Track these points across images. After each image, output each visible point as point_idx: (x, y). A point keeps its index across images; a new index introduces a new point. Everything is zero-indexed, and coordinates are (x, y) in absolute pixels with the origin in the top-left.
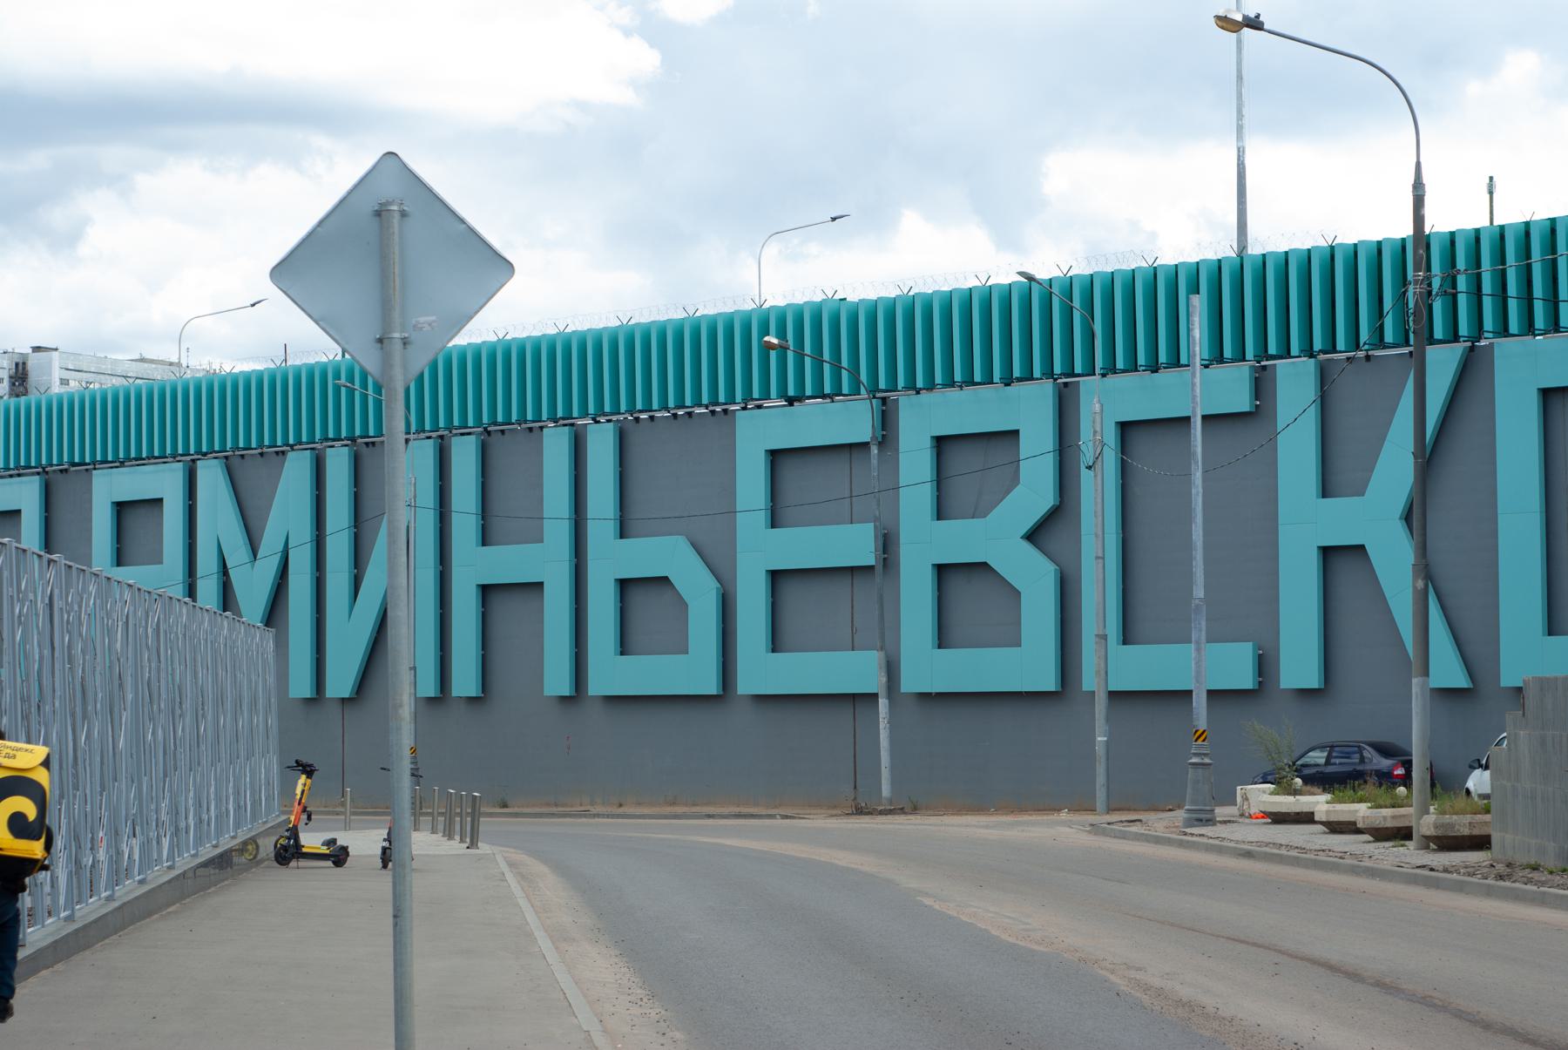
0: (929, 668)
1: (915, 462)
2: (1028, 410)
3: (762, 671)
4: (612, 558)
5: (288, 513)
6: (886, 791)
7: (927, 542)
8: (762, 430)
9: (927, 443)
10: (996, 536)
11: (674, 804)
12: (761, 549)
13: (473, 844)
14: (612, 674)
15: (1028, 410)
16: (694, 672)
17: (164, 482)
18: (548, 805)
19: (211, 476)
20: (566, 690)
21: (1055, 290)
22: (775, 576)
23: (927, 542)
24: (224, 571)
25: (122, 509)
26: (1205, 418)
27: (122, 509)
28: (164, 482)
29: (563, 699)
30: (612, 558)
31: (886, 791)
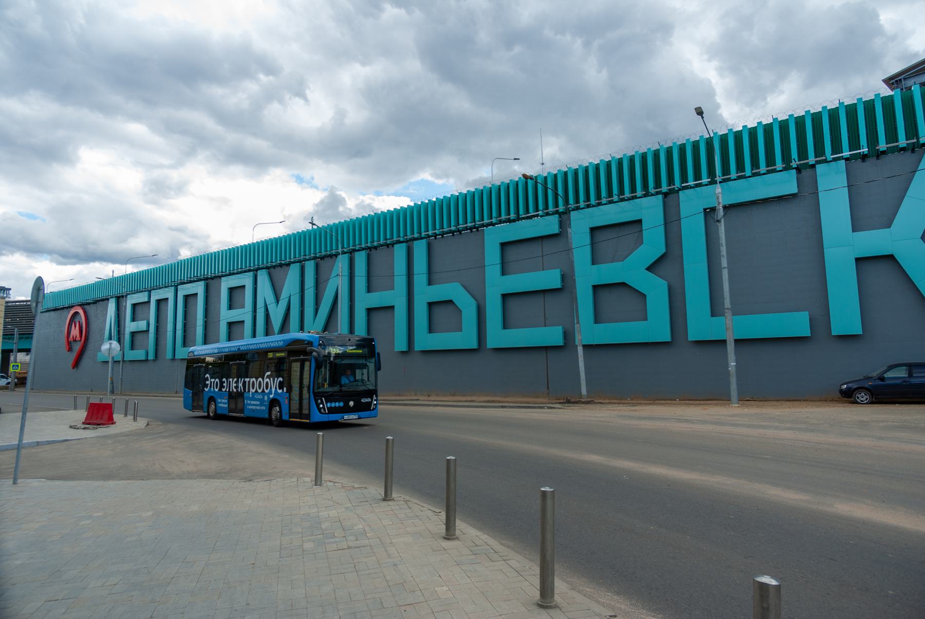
0: (589, 331)
1: (492, 255)
2: (649, 210)
3: (497, 336)
4: (424, 294)
5: (337, 281)
6: (584, 391)
7: (587, 275)
8: (494, 237)
9: (588, 231)
10: (632, 269)
11: (454, 395)
12: (497, 284)
13: (135, 419)
14: (424, 340)
15: (649, 210)
16: (466, 338)
17: (246, 280)
18: (396, 395)
19: (263, 276)
20: (405, 349)
21: (539, 181)
22: (430, 305)
23: (587, 275)
24: (267, 310)
25: (231, 290)
26: (725, 207)
27: (231, 290)
28: (169, 293)
29: (403, 352)
30: (424, 294)
31: (584, 391)
